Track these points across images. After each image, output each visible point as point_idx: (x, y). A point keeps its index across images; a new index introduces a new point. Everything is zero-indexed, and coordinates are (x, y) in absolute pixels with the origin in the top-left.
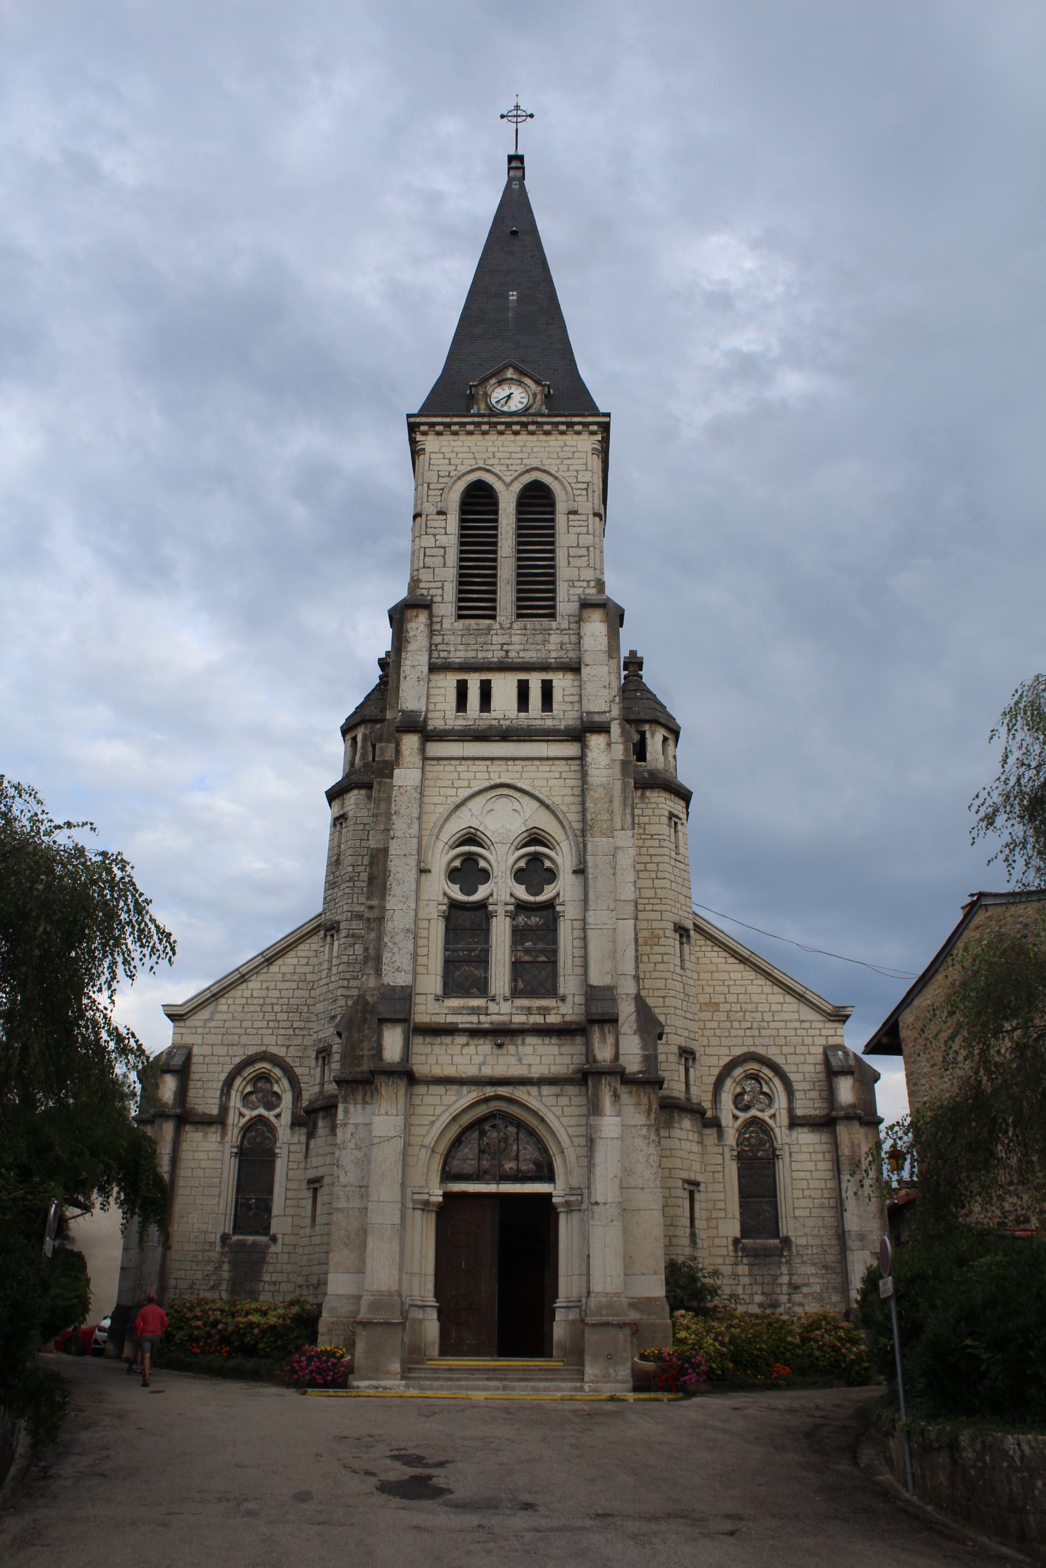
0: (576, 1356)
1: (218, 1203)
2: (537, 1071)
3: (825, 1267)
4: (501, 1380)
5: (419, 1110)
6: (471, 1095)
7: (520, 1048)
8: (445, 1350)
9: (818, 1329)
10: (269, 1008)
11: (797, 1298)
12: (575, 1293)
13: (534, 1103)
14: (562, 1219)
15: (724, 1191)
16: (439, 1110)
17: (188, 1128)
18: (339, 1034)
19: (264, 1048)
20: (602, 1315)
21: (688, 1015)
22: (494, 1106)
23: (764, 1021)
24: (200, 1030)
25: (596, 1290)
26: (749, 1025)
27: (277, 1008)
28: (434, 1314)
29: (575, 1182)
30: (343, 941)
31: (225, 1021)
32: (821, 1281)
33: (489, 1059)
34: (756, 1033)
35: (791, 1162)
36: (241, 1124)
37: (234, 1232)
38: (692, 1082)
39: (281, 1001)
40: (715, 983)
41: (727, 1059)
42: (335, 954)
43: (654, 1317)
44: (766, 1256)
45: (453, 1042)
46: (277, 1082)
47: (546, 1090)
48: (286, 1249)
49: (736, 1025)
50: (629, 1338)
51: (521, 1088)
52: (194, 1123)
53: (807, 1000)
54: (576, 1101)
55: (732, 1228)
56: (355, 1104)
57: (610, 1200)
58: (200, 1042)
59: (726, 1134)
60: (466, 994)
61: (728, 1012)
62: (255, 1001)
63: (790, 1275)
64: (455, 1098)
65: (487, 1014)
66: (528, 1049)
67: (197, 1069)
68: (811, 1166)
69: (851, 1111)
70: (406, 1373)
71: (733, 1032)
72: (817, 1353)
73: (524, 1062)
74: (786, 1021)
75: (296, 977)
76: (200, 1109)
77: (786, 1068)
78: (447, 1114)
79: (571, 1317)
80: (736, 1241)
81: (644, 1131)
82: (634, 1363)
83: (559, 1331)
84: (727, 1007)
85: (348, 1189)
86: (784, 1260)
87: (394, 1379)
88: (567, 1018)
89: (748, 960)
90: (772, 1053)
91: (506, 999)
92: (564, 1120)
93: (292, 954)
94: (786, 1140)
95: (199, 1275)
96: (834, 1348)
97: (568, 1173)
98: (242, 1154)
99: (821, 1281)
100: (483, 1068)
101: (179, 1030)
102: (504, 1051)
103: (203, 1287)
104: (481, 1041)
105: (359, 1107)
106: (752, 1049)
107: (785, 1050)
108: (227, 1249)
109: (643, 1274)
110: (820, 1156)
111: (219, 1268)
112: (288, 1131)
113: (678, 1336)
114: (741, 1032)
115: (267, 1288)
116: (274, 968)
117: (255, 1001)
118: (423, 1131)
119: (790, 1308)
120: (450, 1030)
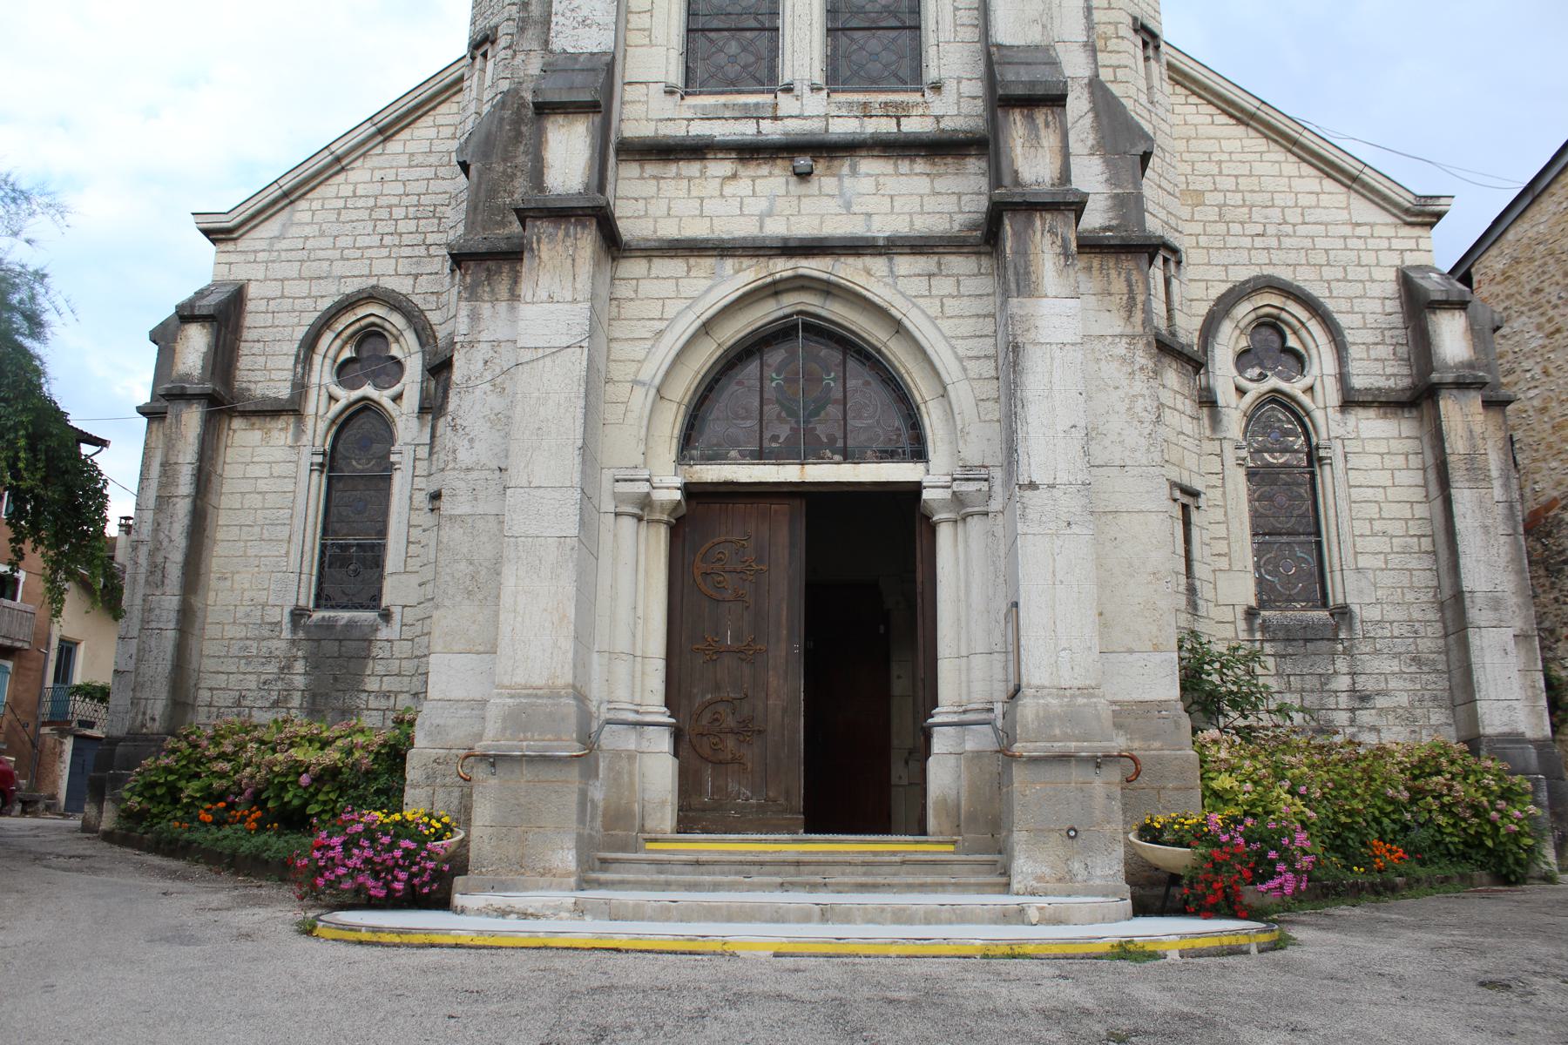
0: (988, 839)
1: (288, 553)
3: (1416, 660)
4: (813, 887)
5: (630, 310)
6: (741, 276)
7: (847, 182)
8: (688, 821)
9: (1439, 773)
10: (384, 214)
11: (1366, 717)
14: (944, 535)
15: (1226, 522)
16: (672, 309)
17: (237, 423)
18: (465, 167)
19: (373, 281)
20: (1054, 739)
21: (1164, 184)
22: (791, 303)
23: (1286, 223)
24: (262, 256)
25: (1035, 681)
26: (1260, 229)
27: (399, 213)
28: (662, 742)
29: (973, 453)
30: (502, 54)
31: (307, 238)
32: (1409, 686)
33: (781, 204)
34: (1274, 242)
35: (1347, 470)
36: (330, 415)
37: (317, 606)
38: (1176, 305)
39: (406, 201)
40: (1195, 157)
41: (1223, 288)
42: (488, 82)
43: (1157, 744)
44: (1307, 640)
45: (702, 173)
46: (397, 340)
47: (904, 264)
48: (408, 633)
49: (1236, 228)
50: (1118, 792)
51: (851, 260)
52: (245, 414)
53: (1365, 185)
54: (970, 285)
55: (1244, 591)
56: (495, 300)
57: (1063, 478)
58: (261, 276)
59: (1225, 419)
60: (732, 85)
61: (1220, 207)
62: (360, 203)
63: (1353, 674)
65: (776, 118)
66: (866, 184)
67: (255, 319)
68: (1384, 478)
69: (1466, 372)
70: (595, 866)
71: (1232, 242)
72: (1442, 820)
73: (855, 209)
74: (1326, 224)
75: (433, 159)
76: (259, 390)
77: (1330, 305)
78: (691, 316)
79: (970, 746)
80: (1251, 614)
81: (1121, 348)
82: (1129, 844)
83: (943, 775)
84: (1220, 197)
85: (474, 475)
86: (1340, 647)
87: (560, 887)
88: (947, 124)
89: (1253, 116)
90: (1305, 279)
91: (815, 89)
92: (945, 325)
93: (427, 120)
94: (1336, 430)
95: (252, 682)
96: (1477, 810)
97: (956, 434)
98: (331, 464)
99: (1409, 686)
100: (768, 221)
101: (225, 258)
102: (813, 186)
103: (259, 703)
104: (765, 169)
105: (502, 307)
106: (1268, 271)
107: (1328, 273)
108: (301, 634)
109: (1131, 651)
110: (1400, 461)
111: (286, 668)
112: (415, 423)
113: (1215, 785)
114: (1247, 242)
115: (373, 703)
116: (394, 146)
117: (360, 203)
118: (639, 351)
119: (1353, 735)
120: (697, 150)
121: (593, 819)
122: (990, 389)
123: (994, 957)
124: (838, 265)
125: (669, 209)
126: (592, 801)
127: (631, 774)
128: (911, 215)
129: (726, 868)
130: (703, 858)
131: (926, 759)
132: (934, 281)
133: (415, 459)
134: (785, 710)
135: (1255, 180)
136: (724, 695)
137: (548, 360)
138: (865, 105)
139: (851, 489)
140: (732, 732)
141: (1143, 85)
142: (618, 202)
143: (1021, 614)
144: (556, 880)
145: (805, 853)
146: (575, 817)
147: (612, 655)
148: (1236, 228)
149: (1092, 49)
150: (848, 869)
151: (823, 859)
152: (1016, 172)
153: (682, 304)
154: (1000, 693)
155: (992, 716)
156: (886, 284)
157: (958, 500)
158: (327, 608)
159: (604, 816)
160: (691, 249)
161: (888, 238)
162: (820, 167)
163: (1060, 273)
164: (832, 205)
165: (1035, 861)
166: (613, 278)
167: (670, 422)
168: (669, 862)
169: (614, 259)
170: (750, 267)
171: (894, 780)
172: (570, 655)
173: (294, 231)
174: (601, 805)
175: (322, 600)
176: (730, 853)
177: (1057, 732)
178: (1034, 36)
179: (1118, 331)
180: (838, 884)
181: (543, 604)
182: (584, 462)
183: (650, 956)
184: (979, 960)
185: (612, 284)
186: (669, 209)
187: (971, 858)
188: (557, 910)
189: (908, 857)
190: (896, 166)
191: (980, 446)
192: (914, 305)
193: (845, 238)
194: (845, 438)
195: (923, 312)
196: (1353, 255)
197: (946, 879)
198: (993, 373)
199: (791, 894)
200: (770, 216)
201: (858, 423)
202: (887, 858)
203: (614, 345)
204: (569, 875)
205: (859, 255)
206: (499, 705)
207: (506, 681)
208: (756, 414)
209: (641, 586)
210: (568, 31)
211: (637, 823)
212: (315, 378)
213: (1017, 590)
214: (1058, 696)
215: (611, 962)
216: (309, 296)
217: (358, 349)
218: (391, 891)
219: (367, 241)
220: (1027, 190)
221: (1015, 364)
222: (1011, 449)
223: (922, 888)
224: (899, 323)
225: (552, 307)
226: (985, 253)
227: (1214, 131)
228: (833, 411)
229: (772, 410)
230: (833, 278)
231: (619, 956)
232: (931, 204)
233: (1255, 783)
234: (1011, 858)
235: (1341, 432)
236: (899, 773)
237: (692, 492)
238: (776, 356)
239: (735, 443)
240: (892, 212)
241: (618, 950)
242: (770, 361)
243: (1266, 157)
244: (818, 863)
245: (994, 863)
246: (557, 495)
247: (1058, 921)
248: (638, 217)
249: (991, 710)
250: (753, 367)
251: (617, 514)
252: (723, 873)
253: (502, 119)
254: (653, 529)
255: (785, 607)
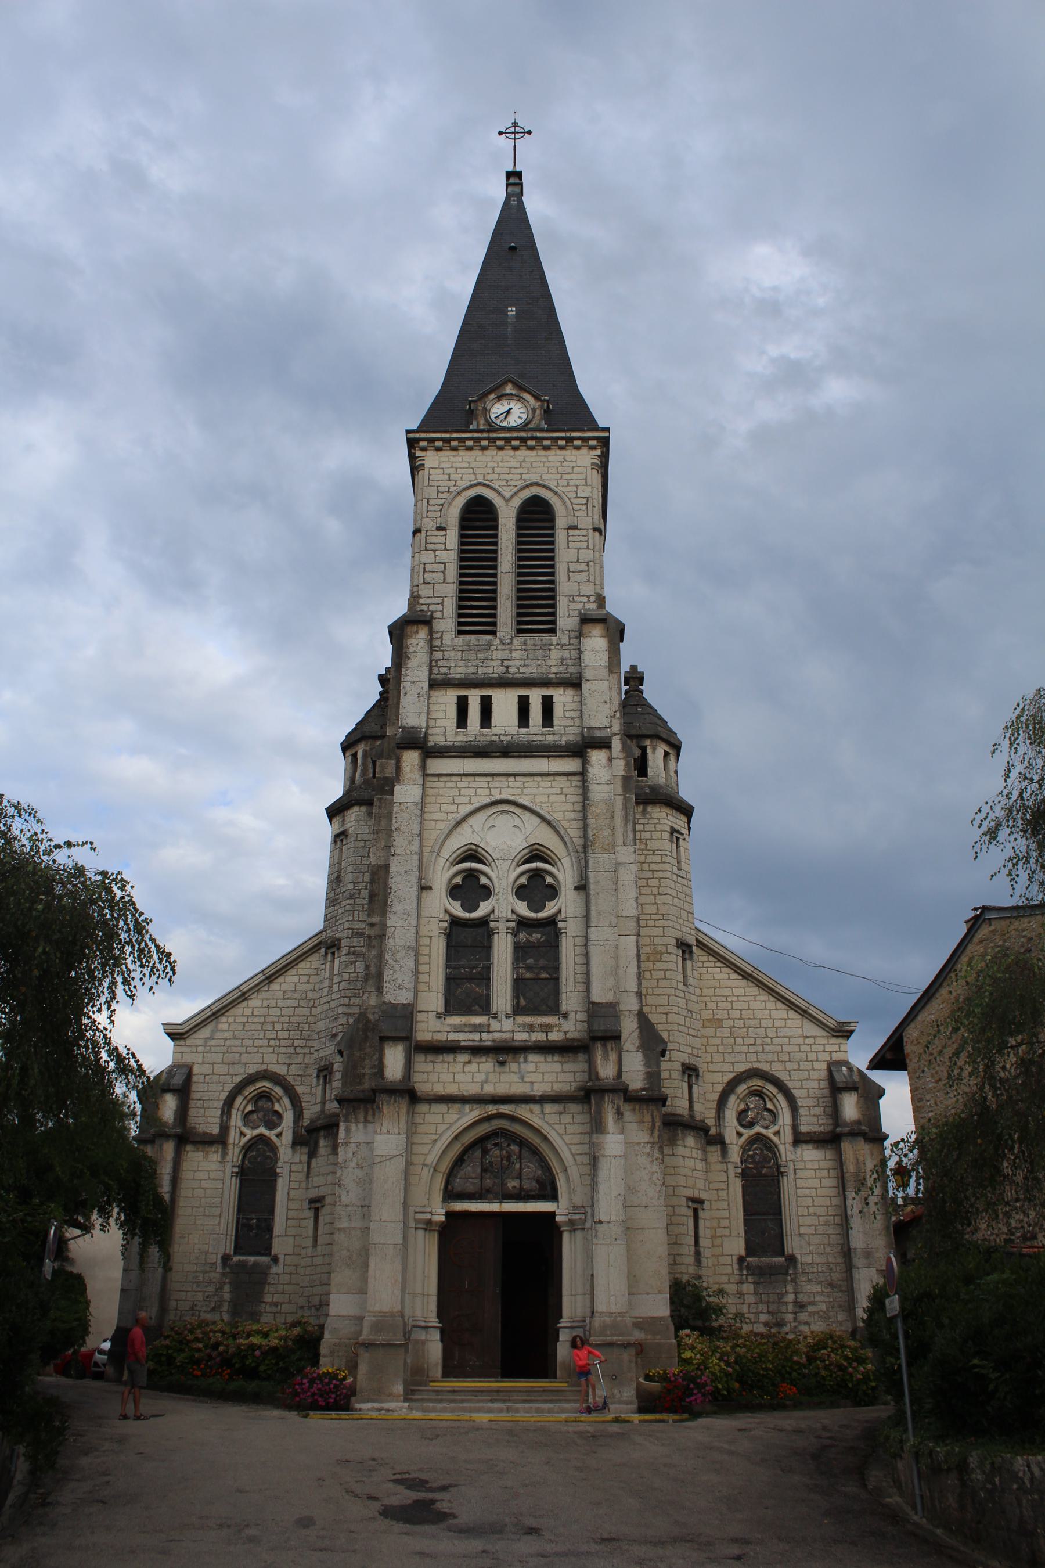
1: (219, 1224)
3: (831, 1285)
4: (504, 1401)
5: (421, 1129)
6: (472, 1114)
7: (523, 1066)
8: (451, 1368)
9: (825, 1348)
11: (803, 1317)
13: (536, 1121)
14: (566, 1237)
15: (729, 1209)
16: (441, 1128)
18: (341, 1053)
19: (264, 1067)
20: (606, 1335)
21: (691, 1032)
22: (496, 1124)
25: (600, 1310)
26: (752, 1041)
27: (278, 1027)
29: (578, 1200)
30: (344, 958)
31: (226, 1039)
32: (827, 1299)
34: (760, 1049)
36: (241, 1144)
37: (235, 1253)
38: (695, 1099)
39: (282, 1019)
42: (336, 972)
43: (658, 1337)
44: (771, 1275)
46: (278, 1101)
47: (549, 1108)
48: (288, 1269)
49: (739, 1041)
51: (523, 1106)
52: (194, 1143)
53: (811, 1015)
54: (579, 1118)
55: (737, 1246)
57: (613, 1218)
58: (200, 1061)
59: (730, 1151)
60: (469, 1012)
61: (731, 1028)
62: (256, 1020)
65: (489, 1032)
66: (531, 1067)
67: (198, 1087)
68: (816, 1183)
70: (409, 1395)
72: (823, 1373)
73: (526, 1079)
74: (789, 1037)
75: (296, 995)
77: (790, 1085)
80: (741, 1260)
81: (648, 1149)
82: (639, 1384)
83: (563, 1351)
85: (350, 1208)
87: (397, 1401)
88: (570, 1036)
89: (750, 975)
90: (776, 1069)
91: (508, 1017)
92: (567, 1138)
93: (293, 971)
95: (200, 1297)
97: (571, 1191)
98: (243, 1173)
99: (827, 1299)
100: (485, 1085)
101: (179, 1049)
102: (506, 1069)
103: (204, 1309)
105: (361, 1126)
106: (756, 1065)
107: (789, 1066)
108: (228, 1270)
109: (648, 1294)
110: (825, 1173)
111: (220, 1289)
113: (683, 1356)
115: (268, 1309)
116: (275, 986)
117: (256, 1020)
118: (425, 1149)
119: (795, 1327)
120: (451, 1048)
133: (290, 1171)
135: (751, 1012)
138: (531, 1026)
141: (680, 977)
147: (414, 1295)
148: (739, 1041)
149: (639, 994)
153: (446, 1126)
158: (243, 1254)
162: (509, 1058)
163: (615, 1122)
173: (218, 1035)
175: (238, 1249)
178: (609, 998)
179: (646, 1140)
181: (386, 1277)
196: (804, 1055)
206: (368, 1320)
207: (371, 1309)
210: (392, 992)
212: (233, 1123)
216: (228, 1074)
217: (256, 1105)
218: (328, 1403)
219: (259, 1043)
227: (730, 983)
233: (702, 1355)
235: (793, 1157)
243: (758, 998)
246: (393, 1225)
251: (416, 1228)
253: (358, 1029)
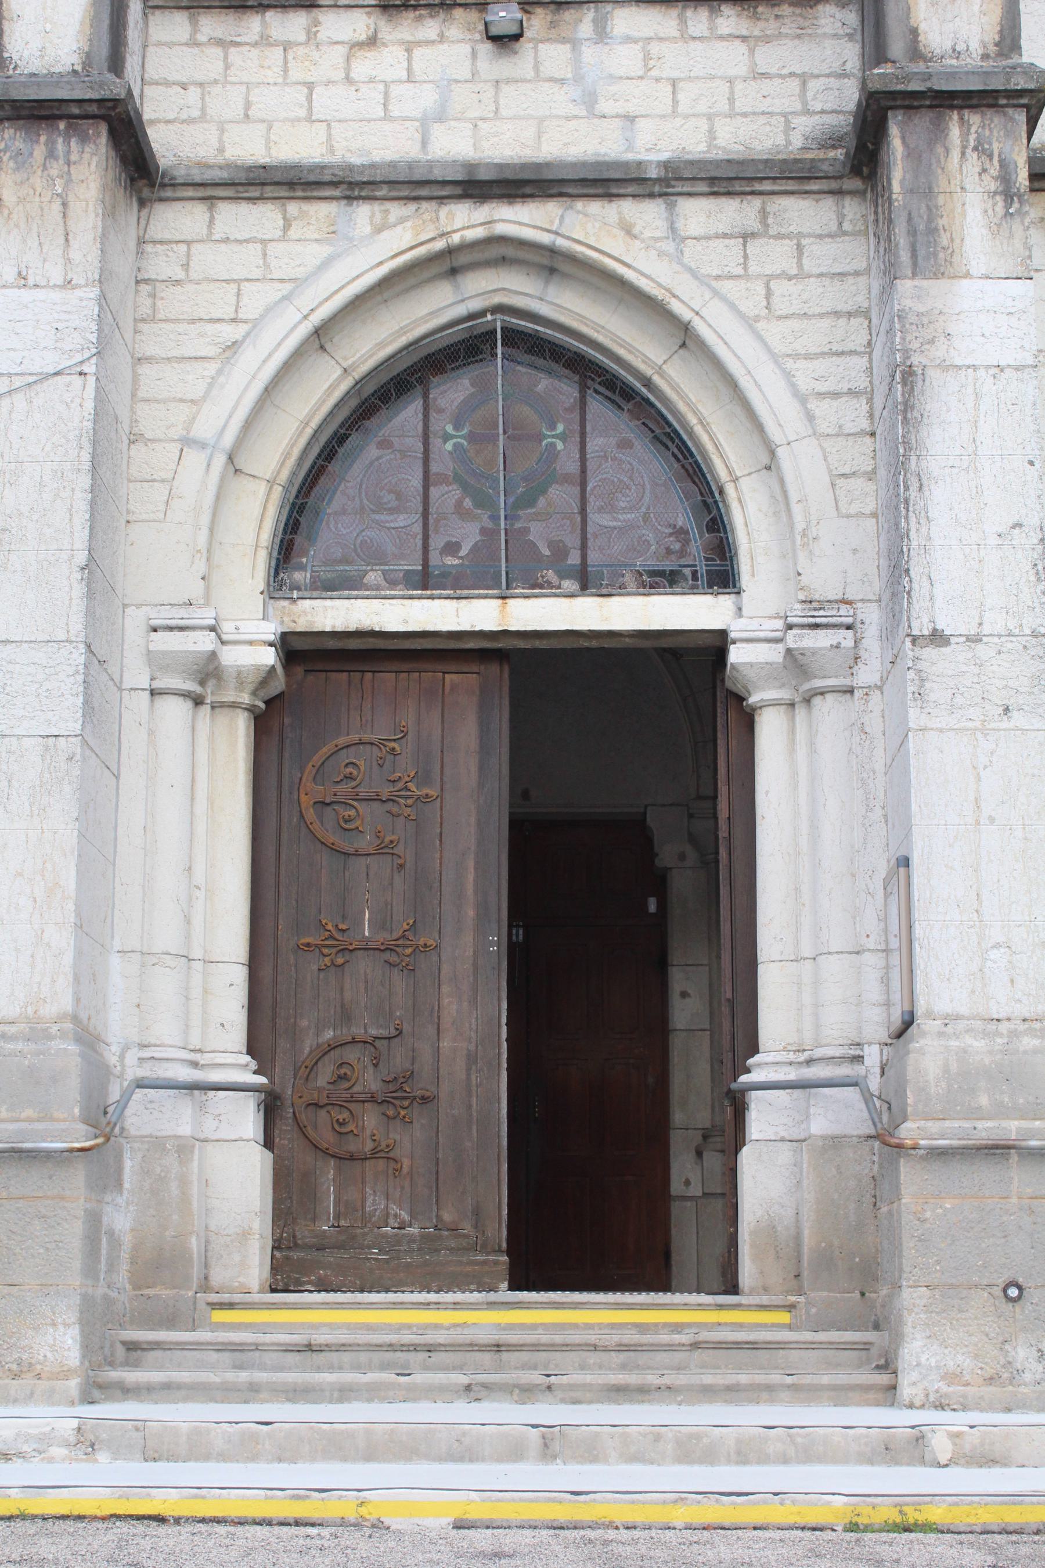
0: (856, 1293)
2: (657, 140)
4: (526, 1393)
5: (174, 302)
6: (394, 235)
7: (589, 53)
8: (298, 1261)
12: (835, 1029)
13: (647, 266)
14: (771, 734)
20: (976, 1113)
25: (942, 1006)
28: (245, 1119)
29: (825, 578)
45: (311, 35)
47: (698, 214)
51: (595, 207)
54: (824, 255)
57: (995, 622)
64: (324, 251)
66: (623, 58)
70: (113, 1359)
73: (605, 106)
79: (819, 1125)
83: (771, 1180)
87: (50, 1398)
92: (775, 332)
97: (794, 539)
100: (437, 131)
104: (430, 28)
118: (192, 381)
121: (111, 1268)
122: (858, 454)
123: (868, 1528)
124: (571, 217)
125: (248, 105)
126: (111, 1233)
127: (184, 1182)
128: (710, 117)
129: (363, 1357)
130: (320, 1338)
131: (737, 1150)
132: (753, 247)
134: (471, 1059)
136: (358, 1031)
137: (19, 398)
139: (594, 644)
140: (373, 1099)
142: (148, 91)
143: (916, 880)
144: (43, 1385)
145: (511, 1327)
146: (77, 1265)
150: (592, 1358)
151: (545, 1339)
152: (914, 32)
153: (273, 292)
154: (876, 1026)
155: (859, 1070)
156: (661, 254)
157: (796, 663)
159: (133, 1261)
160: (291, 185)
161: (666, 165)
162: (537, 23)
163: (995, 229)
164: (561, 100)
165: (944, 1344)
166: (141, 242)
167: (254, 519)
168: (257, 1347)
169: (142, 203)
170: (402, 220)
171: (676, 1187)
172: (68, 959)
174: (127, 1241)
176: (369, 1328)
177: (984, 1100)
180: (572, 1387)
182: (90, 594)
183: (221, 1529)
184: (840, 1535)
185: (140, 253)
186: (248, 105)
187: (822, 1336)
188: (44, 1441)
189: (705, 1335)
190: (683, 21)
191: (841, 563)
192: (716, 293)
193: (584, 164)
194: (584, 547)
195: (732, 306)
197: (776, 1378)
198: (865, 424)
199: (485, 1405)
200: (440, 119)
201: (605, 520)
202: (665, 1338)
203: (144, 369)
204: (65, 1374)
205: (610, 196)
208: (417, 503)
209: (201, 828)
211: (196, 1273)
213: (908, 835)
214: (985, 1034)
215: (146, 1544)
220: (934, 67)
221: (907, 406)
222: (897, 568)
223: (732, 1393)
224: (686, 328)
225: (26, 295)
226: (851, 193)
228: (561, 496)
229: (446, 497)
230: (560, 242)
231: (163, 1530)
232: (749, 97)
234: (897, 1338)
236: (686, 1174)
237: (299, 652)
238: (453, 392)
239: (376, 557)
240: (674, 113)
241: (160, 1519)
242: (442, 402)
244: (536, 1348)
245: (866, 1347)
247: (987, 1459)
248: (190, 121)
249: (858, 1059)
250: (408, 415)
251: (153, 693)
252: (357, 1367)
254: (223, 717)
255: (471, 864)
